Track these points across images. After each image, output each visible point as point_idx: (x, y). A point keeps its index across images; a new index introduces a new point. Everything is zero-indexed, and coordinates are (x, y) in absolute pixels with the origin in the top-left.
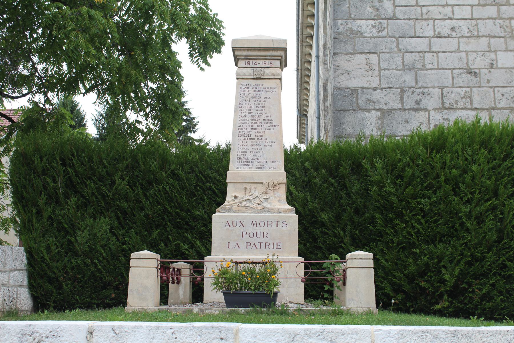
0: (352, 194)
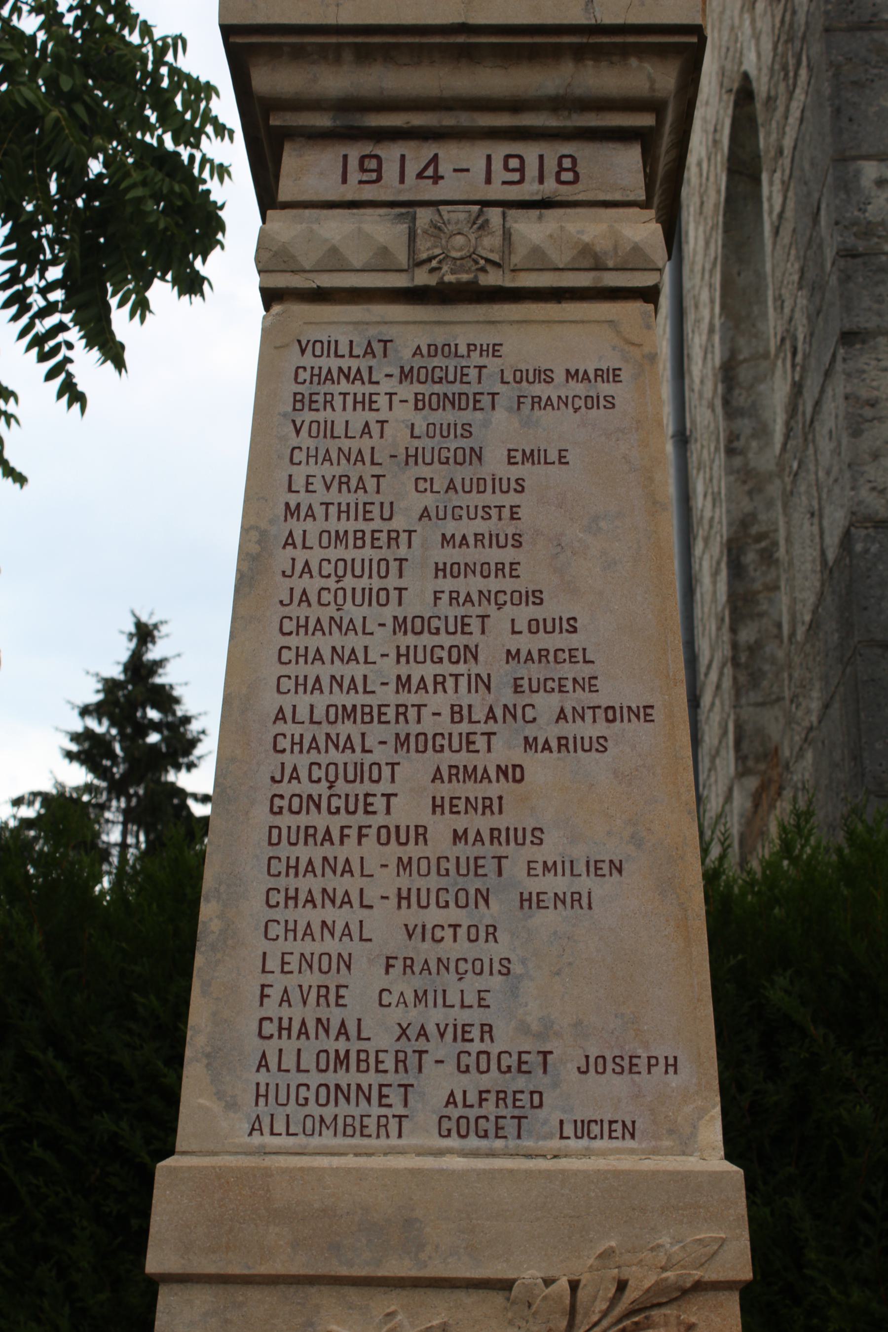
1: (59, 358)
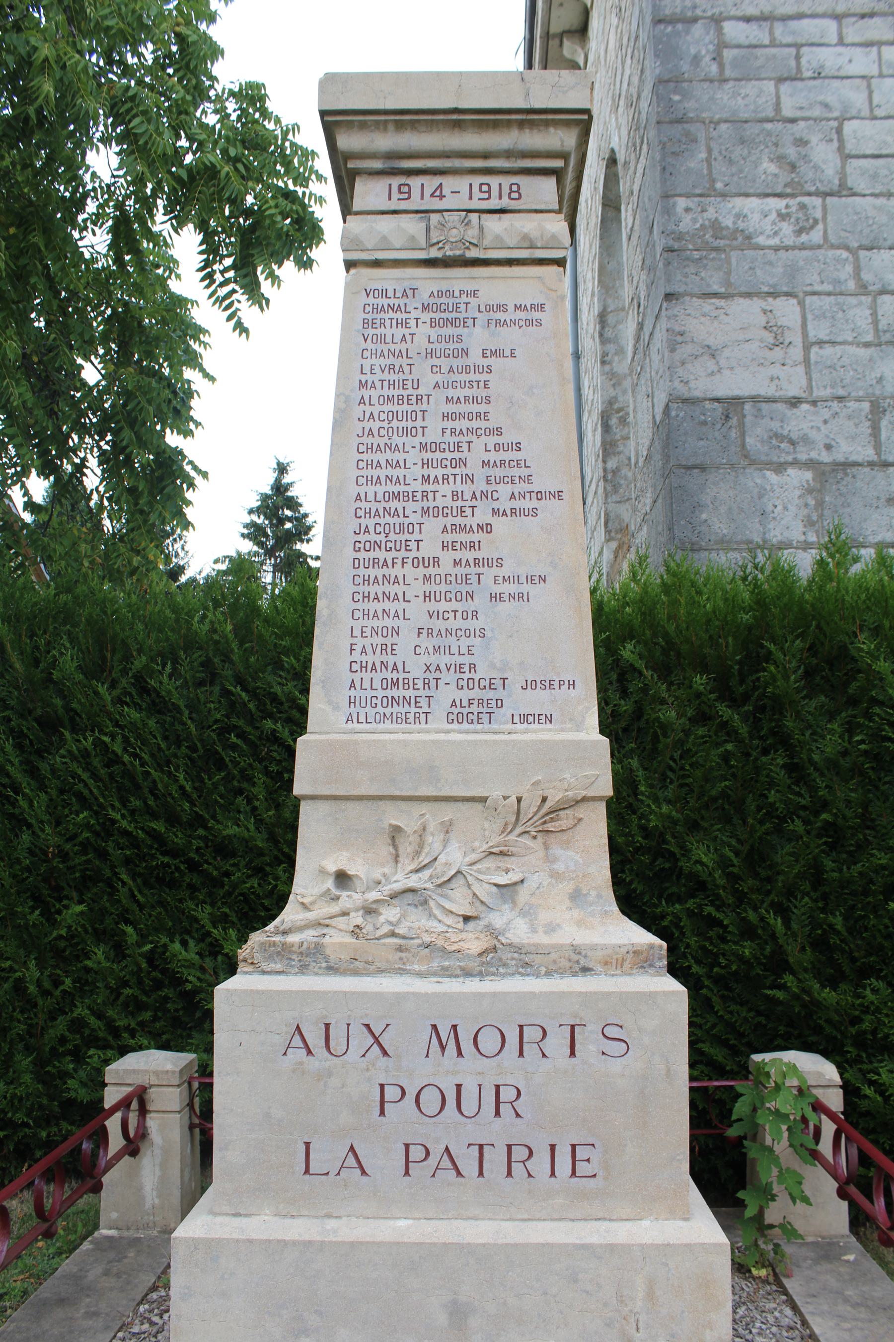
0: (816, 775)
1: (233, 309)
